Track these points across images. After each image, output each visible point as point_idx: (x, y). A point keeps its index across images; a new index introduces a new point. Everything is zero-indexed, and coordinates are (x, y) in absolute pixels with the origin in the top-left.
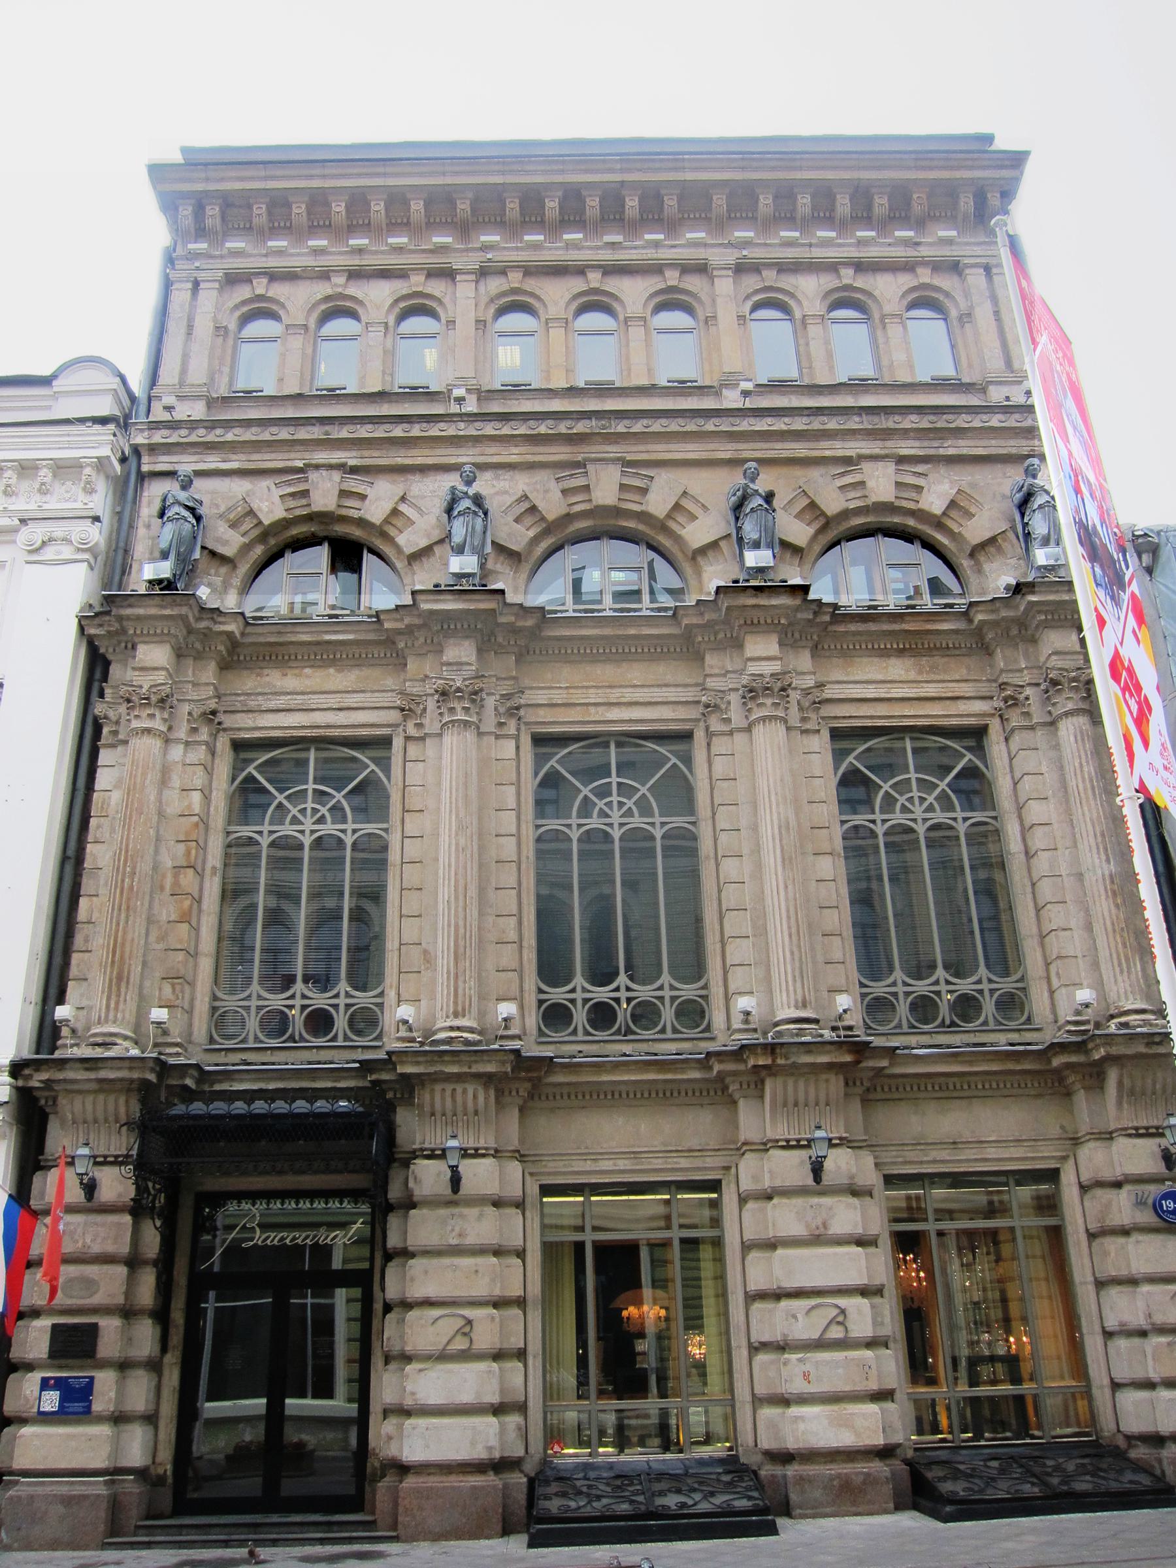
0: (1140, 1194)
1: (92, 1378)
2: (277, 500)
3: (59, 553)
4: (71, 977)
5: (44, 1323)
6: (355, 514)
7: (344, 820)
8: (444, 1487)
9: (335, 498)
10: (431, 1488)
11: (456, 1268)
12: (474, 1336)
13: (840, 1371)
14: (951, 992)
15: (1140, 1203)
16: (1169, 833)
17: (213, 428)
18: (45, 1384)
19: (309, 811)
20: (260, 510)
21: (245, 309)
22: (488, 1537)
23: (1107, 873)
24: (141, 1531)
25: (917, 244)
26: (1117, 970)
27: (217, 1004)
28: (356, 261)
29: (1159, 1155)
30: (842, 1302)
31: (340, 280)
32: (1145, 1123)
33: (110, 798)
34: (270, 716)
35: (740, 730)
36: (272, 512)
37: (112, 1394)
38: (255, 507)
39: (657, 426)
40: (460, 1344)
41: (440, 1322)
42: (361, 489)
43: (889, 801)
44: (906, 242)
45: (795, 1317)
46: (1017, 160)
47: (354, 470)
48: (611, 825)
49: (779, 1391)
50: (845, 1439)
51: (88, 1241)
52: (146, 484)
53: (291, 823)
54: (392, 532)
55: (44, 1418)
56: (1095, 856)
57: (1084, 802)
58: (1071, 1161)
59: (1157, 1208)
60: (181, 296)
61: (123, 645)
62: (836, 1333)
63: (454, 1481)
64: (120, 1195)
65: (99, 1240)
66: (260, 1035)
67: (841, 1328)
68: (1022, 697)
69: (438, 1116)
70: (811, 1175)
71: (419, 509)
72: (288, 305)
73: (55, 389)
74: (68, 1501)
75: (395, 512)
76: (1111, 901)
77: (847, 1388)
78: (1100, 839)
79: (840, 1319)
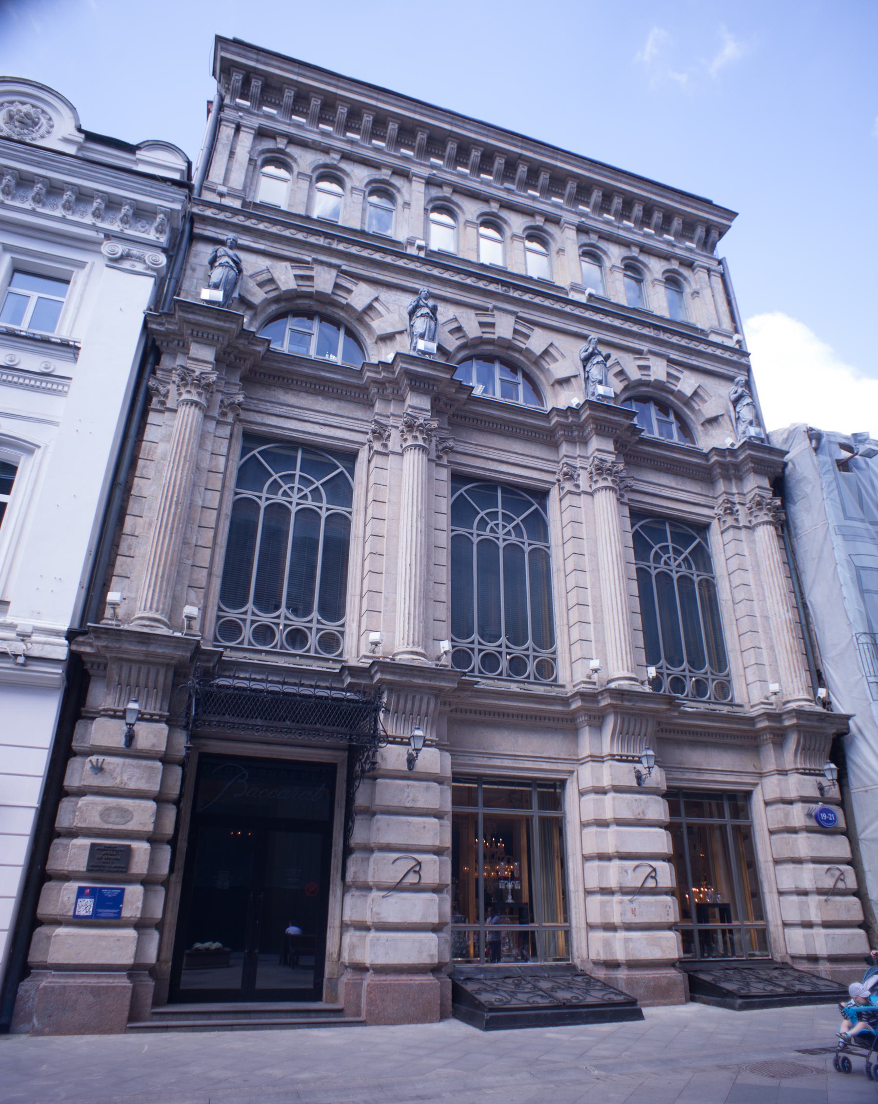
1: (123, 890)
2: (292, 277)
3: (133, 266)
5: (85, 842)
6: (344, 302)
7: (320, 500)
8: (399, 984)
9: (332, 286)
10: (390, 985)
11: (409, 824)
12: (422, 873)
13: (653, 909)
15: (809, 815)
16: (810, 602)
17: (250, 218)
18: (81, 893)
19: (296, 489)
21: (269, 155)
22: (431, 1022)
24: (155, 1017)
25: (674, 246)
26: (794, 674)
27: (222, 614)
28: (347, 147)
29: (816, 787)
30: (654, 864)
32: (813, 767)
33: (156, 448)
34: (274, 418)
35: (586, 493)
36: (287, 283)
37: (140, 904)
38: (276, 276)
40: (412, 879)
41: (398, 862)
42: (348, 285)
43: (657, 557)
44: (669, 243)
45: (626, 871)
46: (732, 215)
47: (345, 272)
48: (498, 539)
49: (612, 921)
50: (656, 954)
51: (125, 778)
52: (194, 243)
53: (283, 495)
54: (367, 319)
55: (78, 921)
56: (781, 607)
58: (759, 787)
59: (817, 818)
60: (227, 131)
61: (176, 342)
62: (651, 884)
63: (404, 979)
64: (154, 745)
65: (134, 779)
66: (252, 640)
67: (654, 881)
69: (400, 713)
70: (635, 780)
71: (388, 309)
72: (299, 160)
73: (138, 156)
74: (96, 991)
75: (370, 307)
77: (657, 920)
79: (653, 874)
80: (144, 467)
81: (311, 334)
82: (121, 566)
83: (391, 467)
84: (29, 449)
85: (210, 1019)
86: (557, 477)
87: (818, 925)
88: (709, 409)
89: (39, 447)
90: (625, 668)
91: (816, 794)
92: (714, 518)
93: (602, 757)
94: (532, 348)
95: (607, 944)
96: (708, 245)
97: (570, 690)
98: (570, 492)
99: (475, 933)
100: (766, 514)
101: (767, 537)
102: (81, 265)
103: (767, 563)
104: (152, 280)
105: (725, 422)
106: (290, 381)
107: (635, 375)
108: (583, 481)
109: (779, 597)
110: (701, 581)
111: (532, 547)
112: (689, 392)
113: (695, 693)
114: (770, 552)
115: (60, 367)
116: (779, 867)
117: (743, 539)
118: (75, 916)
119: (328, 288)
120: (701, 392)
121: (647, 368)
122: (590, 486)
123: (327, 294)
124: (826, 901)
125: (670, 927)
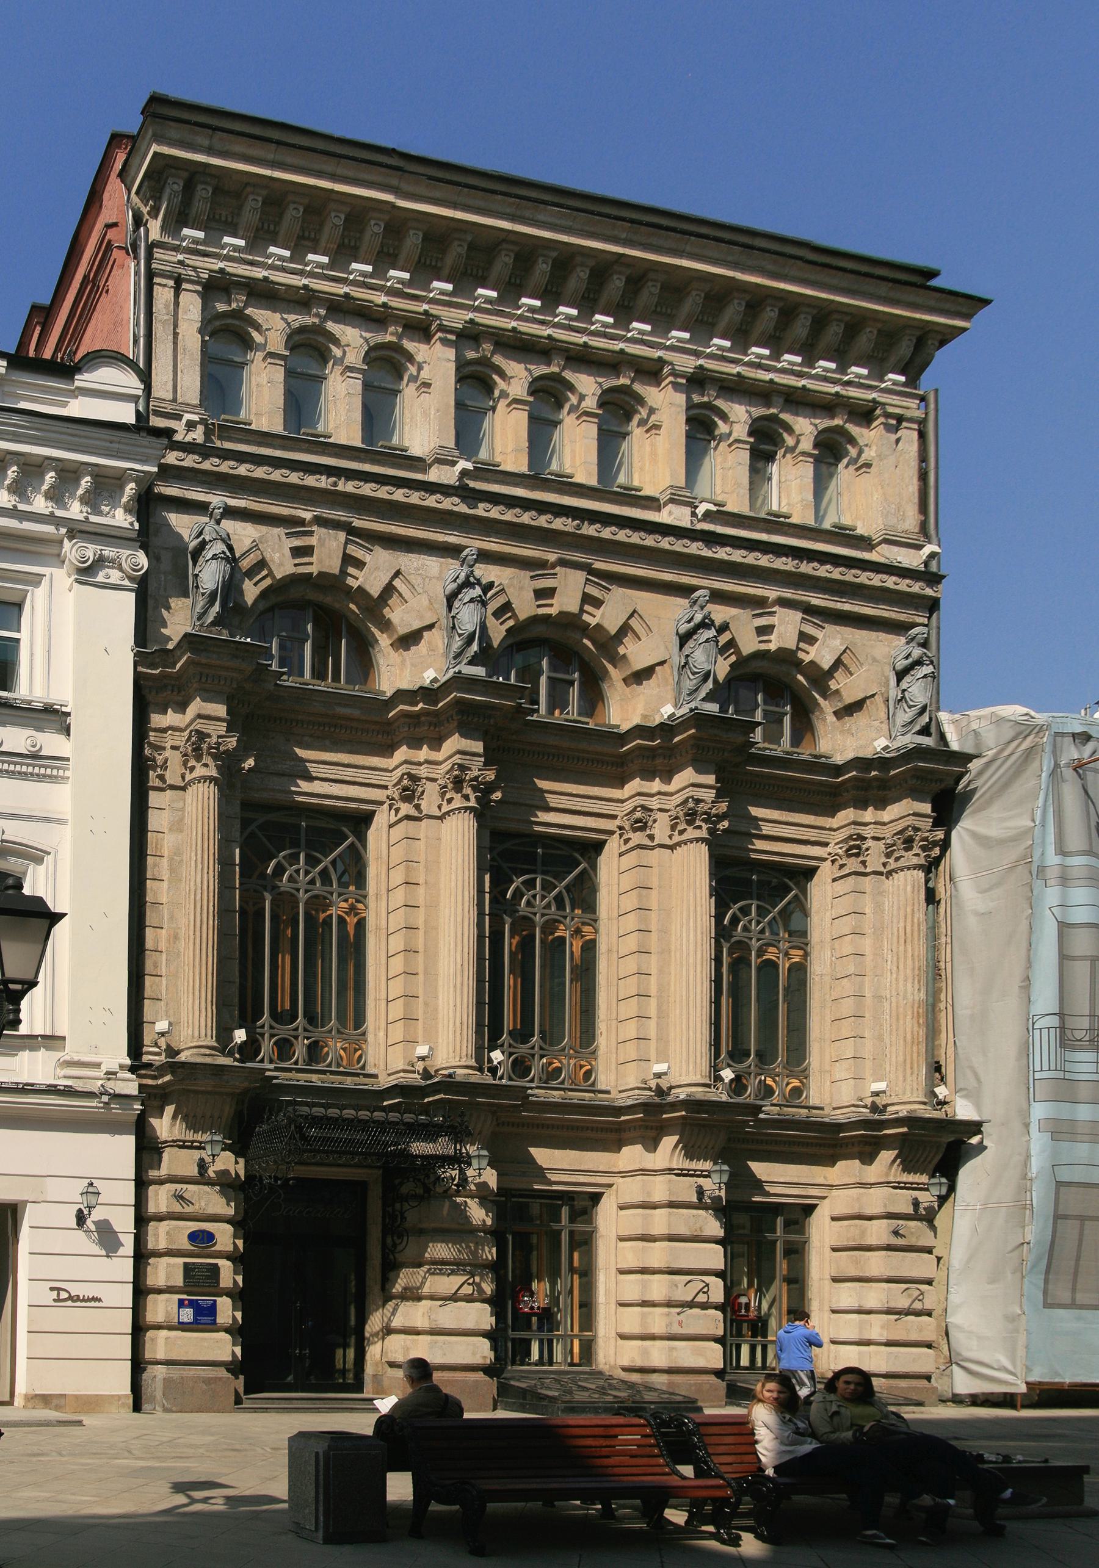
0: (179, 1190)
1: (215, 1301)
2: (288, 553)
10: (448, 1380)
14: (308, 1038)
18: (181, 1304)
20: (273, 561)
21: (217, 323)
23: (917, 998)
26: (909, 1071)
30: (706, 1278)
38: (267, 556)
39: (623, 535)
45: (676, 1286)
56: (909, 985)
57: (908, 941)
60: (163, 295)
62: (702, 1298)
63: (459, 1375)
68: (864, 847)
76: (915, 1021)
78: (917, 972)
80: (155, 865)
81: (572, 683)
82: (151, 987)
83: (427, 837)
85: (342, 1404)
86: (618, 822)
88: (848, 687)
89: (49, 853)
90: (698, 1073)
91: (910, 1210)
92: (825, 860)
94: (606, 624)
95: (645, 1352)
96: (913, 369)
97: (385, 1081)
98: (408, 817)
99: (548, 1340)
100: (917, 855)
101: (909, 888)
102: (36, 580)
103: (902, 925)
104: (132, 596)
105: (876, 708)
106: (294, 724)
107: (749, 644)
108: (661, 830)
109: (909, 972)
111: (546, 918)
112: (826, 663)
113: (306, 1058)
114: (909, 910)
115: (51, 743)
117: (868, 890)
118: (179, 1323)
119: (333, 566)
120: (846, 659)
121: (307, 551)
122: (440, 807)
123: (334, 575)
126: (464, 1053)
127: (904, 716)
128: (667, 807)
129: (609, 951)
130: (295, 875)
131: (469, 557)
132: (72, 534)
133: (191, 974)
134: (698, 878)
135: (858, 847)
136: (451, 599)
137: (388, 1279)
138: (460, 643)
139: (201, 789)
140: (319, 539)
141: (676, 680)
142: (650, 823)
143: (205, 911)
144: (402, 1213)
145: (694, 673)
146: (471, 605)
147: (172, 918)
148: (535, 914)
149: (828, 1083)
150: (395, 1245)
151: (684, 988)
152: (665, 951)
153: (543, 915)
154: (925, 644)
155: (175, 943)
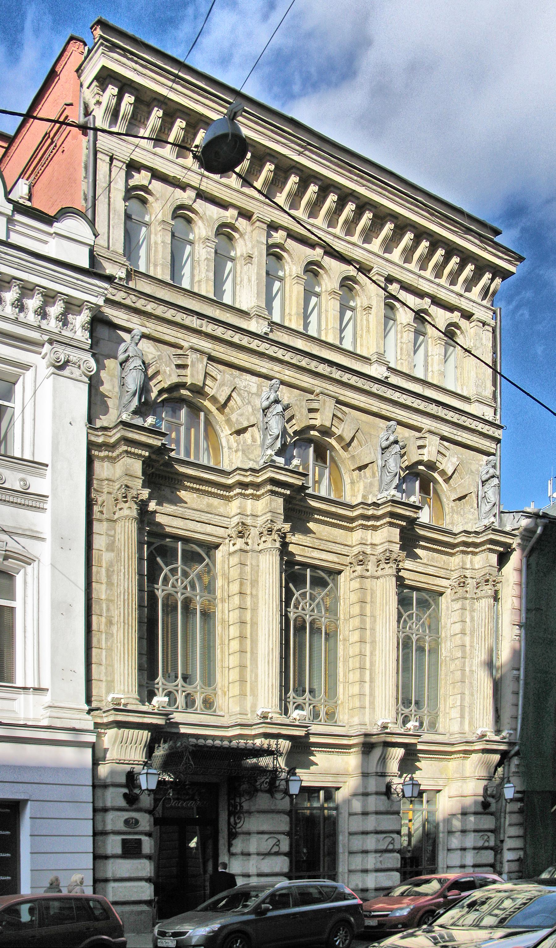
4: (93, 662)
31: (191, 194)
40: (276, 849)
62: (391, 847)
79: (392, 842)
83: (252, 564)
84: (28, 561)
86: (229, 531)
87: (254, 875)
93: (368, 774)
106: (176, 482)
110: (296, 618)
111: (312, 617)
116: (351, 837)
124: (477, 853)
125: (397, 870)
126: (274, 704)
127: (485, 508)
128: (376, 553)
129: (344, 640)
130: (175, 582)
131: (275, 385)
132: (51, 342)
133: (122, 649)
134: (391, 597)
135: (464, 583)
136: (265, 410)
137: (232, 844)
138: (270, 440)
139: (127, 524)
140: (192, 362)
141: (380, 475)
142: (366, 563)
143: (130, 607)
144: (240, 804)
145: (389, 472)
146: (277, 417)
147: (108, 610)
148: (306, 615)
149: (448, 720)
150: (236, 824)
151: (384, 666)
152: (373, 642)
153: (311, 616)
154: (494, 467)
155: (110, 627)
